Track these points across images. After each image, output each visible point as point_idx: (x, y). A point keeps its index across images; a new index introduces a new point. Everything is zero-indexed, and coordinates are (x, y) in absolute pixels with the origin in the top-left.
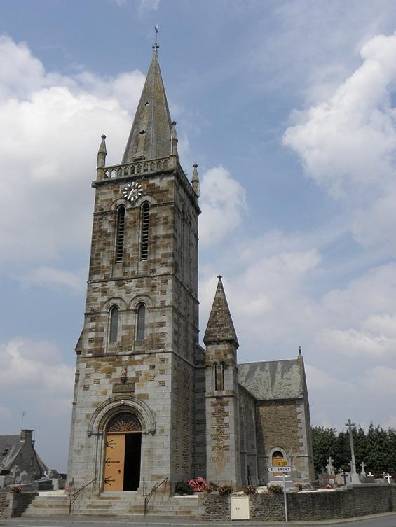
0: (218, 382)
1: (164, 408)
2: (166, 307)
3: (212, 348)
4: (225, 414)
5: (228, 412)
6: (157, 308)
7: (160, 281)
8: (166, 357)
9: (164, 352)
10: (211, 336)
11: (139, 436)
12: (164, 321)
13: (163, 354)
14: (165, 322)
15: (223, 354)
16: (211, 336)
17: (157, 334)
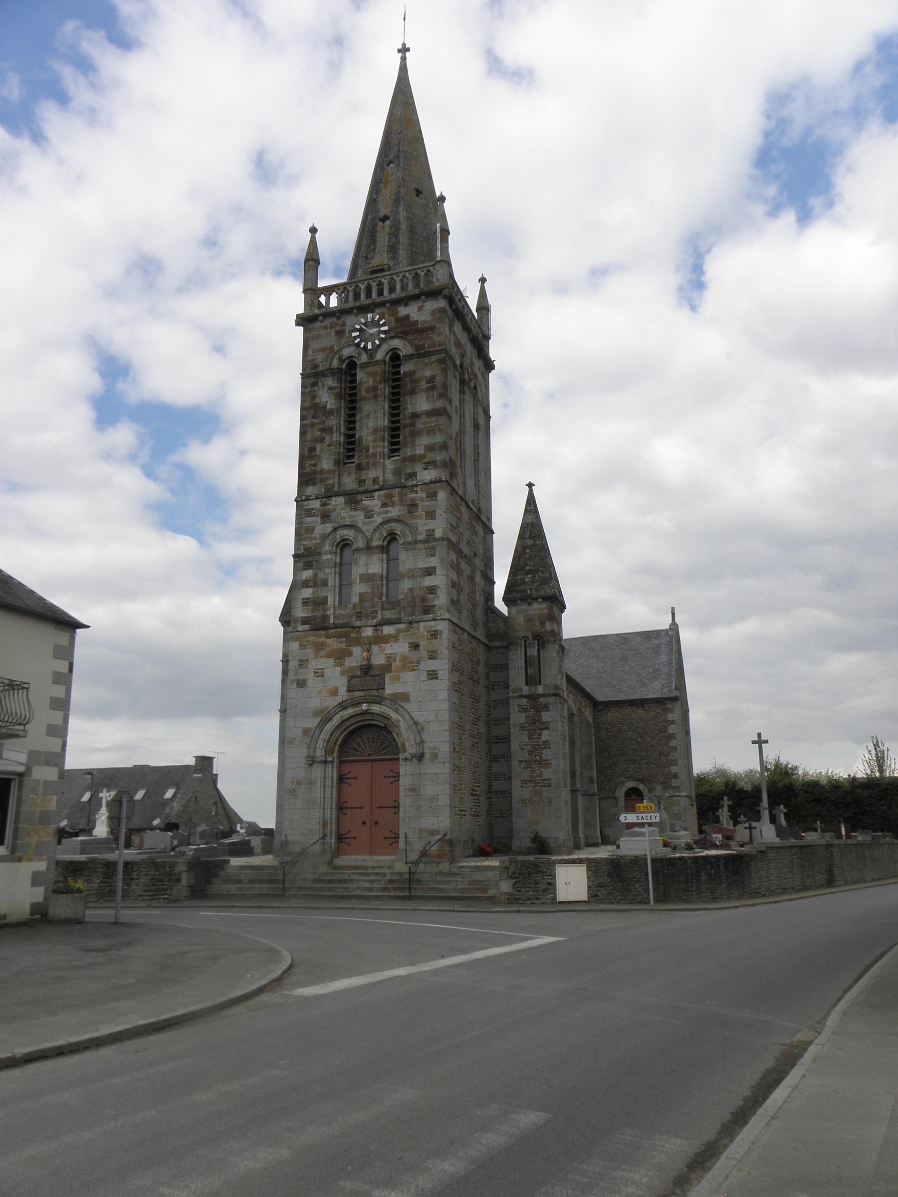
0: (529, 671)
1: (437, 716)
2: (436, 540)
6: (421, 542)
7: (424, 495)
8: (439, 628)
9: (434, 620)
10: (517, 592)
13: (433, 623)
14: (435, 568)
15: (537, 622)
17: (420, 588)
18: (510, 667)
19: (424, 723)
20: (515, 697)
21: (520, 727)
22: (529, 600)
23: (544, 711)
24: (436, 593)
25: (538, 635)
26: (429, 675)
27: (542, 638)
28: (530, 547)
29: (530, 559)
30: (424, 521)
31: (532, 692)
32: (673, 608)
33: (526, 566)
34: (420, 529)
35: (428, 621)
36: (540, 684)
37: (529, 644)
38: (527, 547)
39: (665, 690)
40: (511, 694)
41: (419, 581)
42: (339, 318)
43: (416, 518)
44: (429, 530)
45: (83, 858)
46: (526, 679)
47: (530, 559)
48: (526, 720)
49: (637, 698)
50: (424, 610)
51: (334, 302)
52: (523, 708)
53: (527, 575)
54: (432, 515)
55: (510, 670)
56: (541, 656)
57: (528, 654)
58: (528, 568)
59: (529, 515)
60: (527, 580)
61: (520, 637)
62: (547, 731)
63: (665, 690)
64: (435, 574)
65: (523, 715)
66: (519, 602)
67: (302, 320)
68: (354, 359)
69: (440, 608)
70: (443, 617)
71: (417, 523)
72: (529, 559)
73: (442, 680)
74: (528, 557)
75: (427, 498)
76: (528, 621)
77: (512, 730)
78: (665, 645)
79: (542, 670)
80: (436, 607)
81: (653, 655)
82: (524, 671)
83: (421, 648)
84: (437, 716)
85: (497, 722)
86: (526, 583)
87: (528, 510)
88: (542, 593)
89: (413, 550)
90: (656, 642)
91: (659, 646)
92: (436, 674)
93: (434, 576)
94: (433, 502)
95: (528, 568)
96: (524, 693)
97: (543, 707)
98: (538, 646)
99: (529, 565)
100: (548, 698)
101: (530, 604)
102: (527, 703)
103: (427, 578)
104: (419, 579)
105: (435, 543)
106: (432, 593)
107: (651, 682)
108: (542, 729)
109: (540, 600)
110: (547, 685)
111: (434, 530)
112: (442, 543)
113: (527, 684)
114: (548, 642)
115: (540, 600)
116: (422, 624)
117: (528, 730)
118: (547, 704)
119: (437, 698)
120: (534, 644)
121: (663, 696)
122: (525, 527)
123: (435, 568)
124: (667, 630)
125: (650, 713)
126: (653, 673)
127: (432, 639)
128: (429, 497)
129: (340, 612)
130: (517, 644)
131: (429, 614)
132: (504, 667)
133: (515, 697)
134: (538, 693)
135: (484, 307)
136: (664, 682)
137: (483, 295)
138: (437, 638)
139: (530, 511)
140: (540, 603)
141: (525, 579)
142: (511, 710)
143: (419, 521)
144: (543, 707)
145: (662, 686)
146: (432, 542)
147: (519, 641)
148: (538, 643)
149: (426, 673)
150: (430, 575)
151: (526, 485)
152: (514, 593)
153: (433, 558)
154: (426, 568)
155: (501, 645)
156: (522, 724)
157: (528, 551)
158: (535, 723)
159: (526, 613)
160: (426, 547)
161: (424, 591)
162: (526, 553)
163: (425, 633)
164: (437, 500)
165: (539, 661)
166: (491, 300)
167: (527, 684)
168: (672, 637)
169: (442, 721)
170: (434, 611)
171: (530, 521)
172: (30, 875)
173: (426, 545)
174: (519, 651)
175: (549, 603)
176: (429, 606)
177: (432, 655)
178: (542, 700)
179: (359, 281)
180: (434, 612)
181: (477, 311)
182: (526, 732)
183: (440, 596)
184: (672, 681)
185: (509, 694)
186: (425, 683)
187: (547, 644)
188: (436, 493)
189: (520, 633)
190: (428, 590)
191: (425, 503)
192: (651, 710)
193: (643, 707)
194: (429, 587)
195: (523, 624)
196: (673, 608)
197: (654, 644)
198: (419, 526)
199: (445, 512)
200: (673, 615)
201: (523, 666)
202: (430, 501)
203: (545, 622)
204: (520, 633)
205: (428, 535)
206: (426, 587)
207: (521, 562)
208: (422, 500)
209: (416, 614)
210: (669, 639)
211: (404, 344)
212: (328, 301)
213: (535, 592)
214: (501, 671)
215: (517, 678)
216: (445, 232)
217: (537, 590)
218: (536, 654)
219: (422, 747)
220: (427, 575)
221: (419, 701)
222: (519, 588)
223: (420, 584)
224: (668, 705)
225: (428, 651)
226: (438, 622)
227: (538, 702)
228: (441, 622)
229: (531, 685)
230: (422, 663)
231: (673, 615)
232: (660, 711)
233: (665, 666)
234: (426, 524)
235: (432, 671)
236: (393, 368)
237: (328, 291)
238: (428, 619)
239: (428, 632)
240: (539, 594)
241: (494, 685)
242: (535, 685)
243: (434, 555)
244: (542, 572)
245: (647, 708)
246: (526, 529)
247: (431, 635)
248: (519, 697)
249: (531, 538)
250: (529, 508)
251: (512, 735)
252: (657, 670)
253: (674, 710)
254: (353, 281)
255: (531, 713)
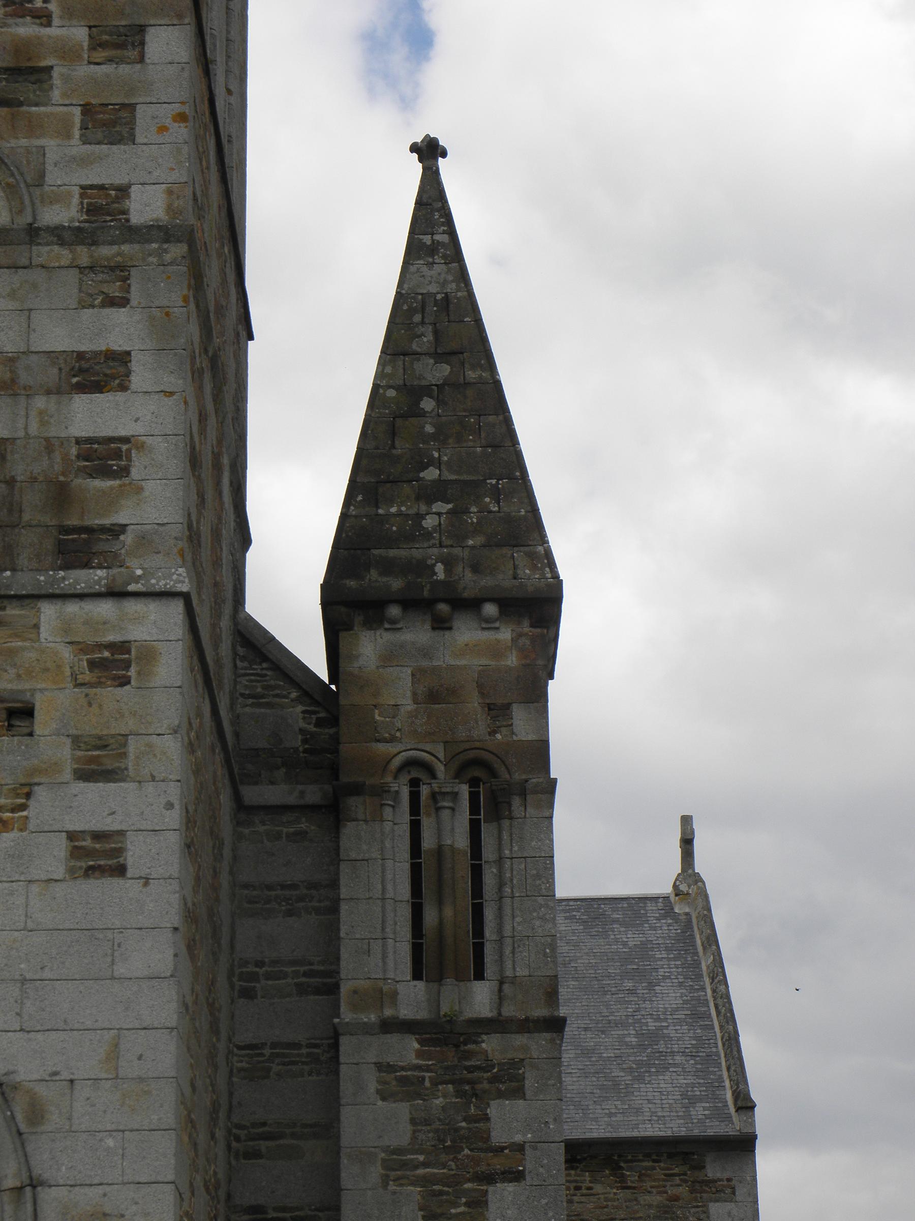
0: (430, 917)
1: (114, 1053)
2: (133, 233)
3: (389, 658)
4: (498, 1163)
5: (520, 1148)
6: (58, 234)
7: (80, 34)
8: (137, 633)
9: (117, 594)
10: (388, 567)
11: (483, 944)
12: (117, 344)
13: (105, 609)
14: (123, 358)
15: (473, 704)
16: (388, 567)
17: (49, 445)
18: (344, 892)
19: (41, 1090)
20: (366, 1029)
21: (387, 1165)
22: (443, 607)
23: (501, 1095)
24: (125, 471)
25: (478, 762)
26: (76, 852)
27: (493, 773)
28: (439, 391)
29: (441, 436)
30: (76, 147)
31: (445, 1009)
32: (686, 821)
33: (425, 467)
34: (54, 177)
35: (81, 596)
36: (480, 975)
37: (434, 796)
38: (426, 390)
39: (700, 1110)
40: (347, 1015)
41: (41, 413)
43: (34, 128)
44: (102, 187)
46: (417, 951)
47: (441, 436)
48: (414, 1138)
49: (595, 1135)
50: (60, 543)
52: (403, 1081)
53: (430, 501)
54: (114, 123)
55: (344, 907)
56: (488, 852)
57: (428, 842)
58: (431, 474)
59: (431, 265)
60: (429, 522)
61: (396, 762)
62: (510, 1187)
63: (700, 1110)
64: (123, 388)
65: (403, 1110)
66: (394, 611)
69: (144, 542)
70: (161, 585)
71: (42, 150)
72: (434, 437)
73: (146, 881)
74: (429, 429)
75: (92, 48)
76: (433, 697)
77: (346, 1180)
78: (668, 950)
79: (489, 914)
80: (128, 538)
81: (629, 984)
82: (405, 913)
83: (43, 723)
84: (114, 1053)
85: (263, 1145)
86: (428, 535)
87: (422, 244)
88: (502, 580)
89: (16, 267)
90: (633, 938)
91: (644, 949)
92: (119, 851)
93: (120, 396)
94: (125, 70)
95: (431, 474)
96: (406, 1012)
97: (494, 1080)
98: (474, 808)
99: (438, 464)
100: (519, 1040)
101: (441, 624)
103: (81, 403)
104: (40, 402)
105: (125, 248)
106: (105, 472)
107: (640, 1079)
108: (489, 1179)
109: (490, 609)
110: (514, 980)
111: (123, 191)
112: (160, 253)
113: (417, 975)
114: (523, 794)
115: (490, 609)
116: (48, 612)
117: (425, 1181)
118: (516, 1064)
119: (120, 970)
120: (455, 796)
121: (696, 1132)
122: (412, 311)
123: (123, 358)
124: (666, 898)
125: (645, 1199)
126: (642, 1047)
127: (99, 684)
128: (102, 45)
130: (380, 792)
131: (87, 565)
132: (301, 899)
133: (366, 1029)
134: (469, 1014)
136: (690, 1080)
138: (124, 682)
139: (433, 249)
140: (488, 624)
141: (421, 517)
142: (346, 1088)
143: (50, 143)
144: (494, 1080)
145: (684, 1095)
146: (112, 243)
147: (389, 779)
148: (474, 798)
149: (61, 846)
150: (98, 387)
151: (414, 148)
152: (374, 574)
153: (119, 315)
154: (81, 356)
155: (292, 800)
156: (398, 1151)
157: (428, 404)
158: (455, 1149)
159: (425, 663)
160: (84, 261)
161: (65, 458)
162: (422, 414)
163: (67, 654)
164: (141, 59)
165: (477, 872)
167: (417, 975)
168: (689, 921)
169: (141, 1080)
170: (116, 555)
171: (433, 289)
172: (680, 817)
173: (84, 255)
174: (388, 826)
175: (526, 627)
176: (89, 530)
177: (91, 760)
178: (491, 1044)
180: (112, 560)
182: (415, 1190)
183: (150, 487)
184: (720, 1080)
185: (338, 1016)
186: (59, 890)
187: (516, 802)
188: (141, 29)
189: (392, 749)
190: (85, 456)
191: (83, 71)
192: (648, 1184)
193: (616, 1169)
194: (90, 440)
195: (408, 705)
196: (686, 821)
197: (625, 944)
198: (49, 167)
199: (181, 118)
200: (687, 843)
201: (404, 890)
202: (110, 60)
203: (507, 707)
204: (392, 749)
205: (92, 210)
206: (78, 441)
207: (402, 447)
208: (68, 53)
209: (23, 560)
210: (676, 930)
213: (469, 575)
214: (290, 913)
215: (376, 947)
217: (476, 568)
218: (462, 842)
219: (29, 1207)
220: (82, 388)
221: (24, 981)
222: (392, 553)
223: (43, 423)
224: (714, 1170)
225: (76, 741)
226: (133, 607)
227: (468, 1055)
228: (152, 610)
229: (439, 979)
230: (40, 793)
231: (687, 843)
232: (683, 1191)
233: (680, 1022)
234: (84, 162)
235: (98, 836)
238: (81, 587)
239: (82, 648)
240: (486, 581)
241: (254, 977)
242: (461, 977)
243: (122, 302)
244: (496, 493)
245: (632, 1177)
246: (417, 318)
247: (92, 664)
248: (389, 1026)
249: (440, 356)
250: (427, 239)
251: (346, 1197)
252: (655, 1036)
253: (733, 1189)
255: (439, 1102)
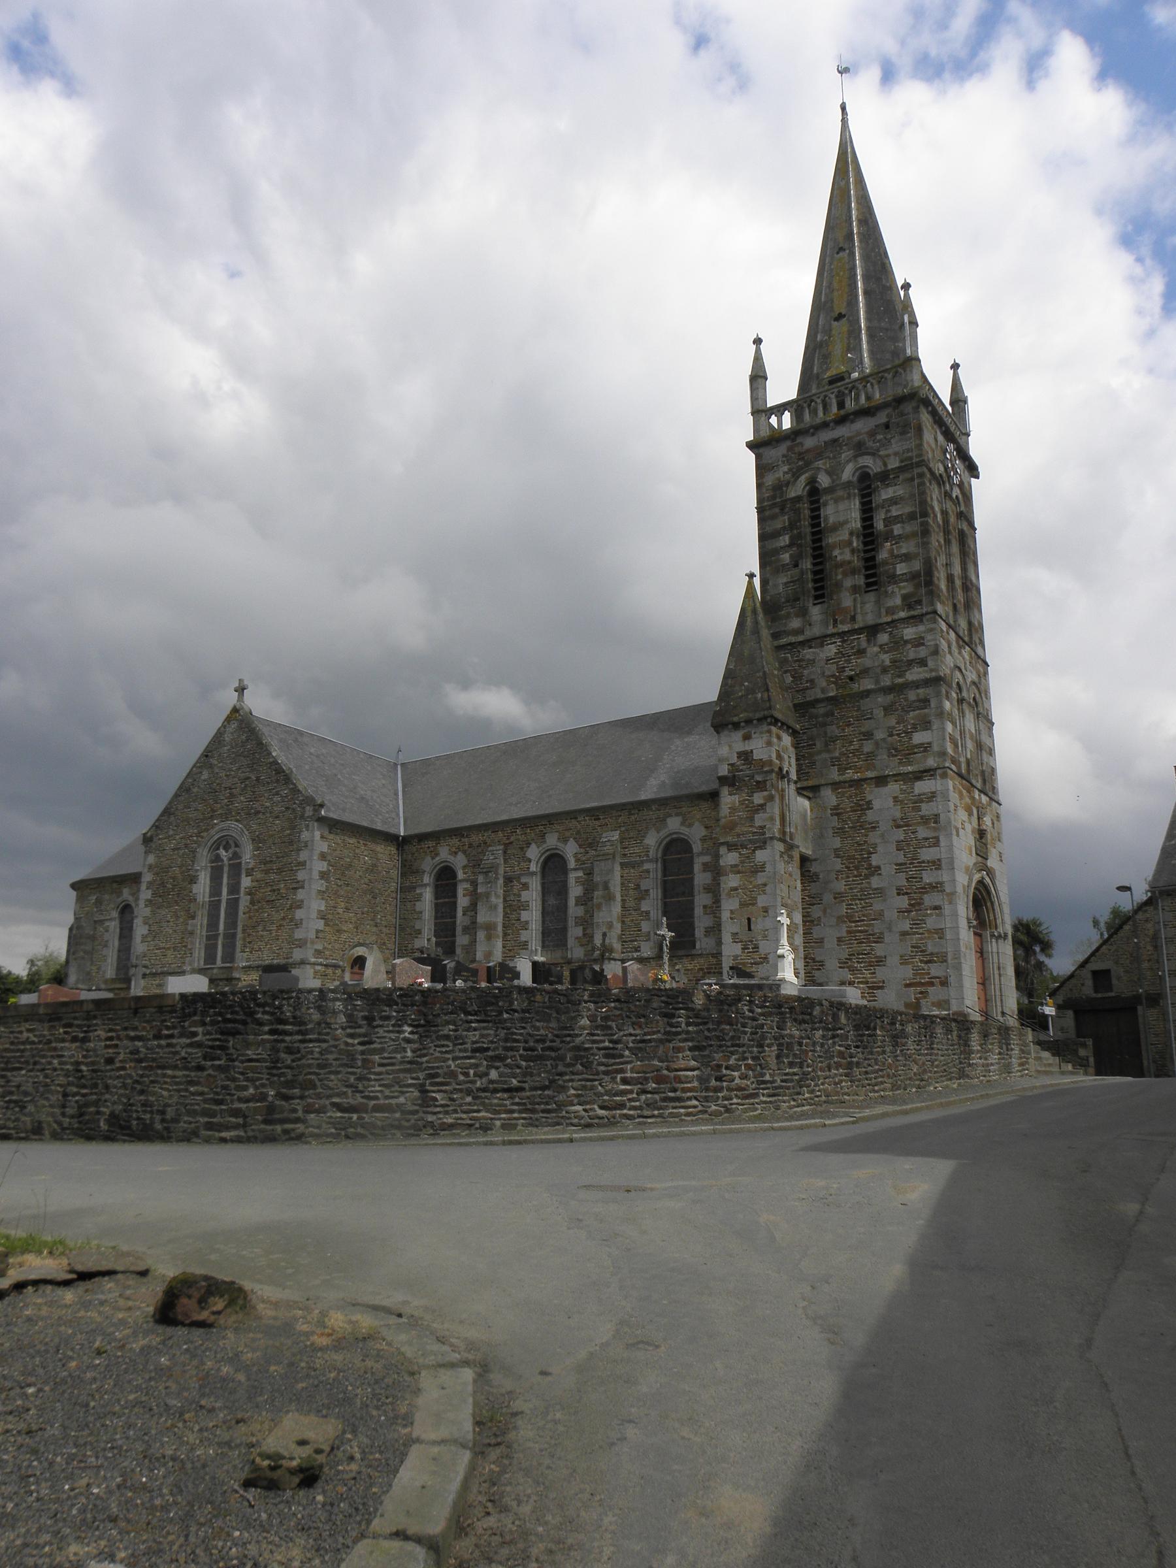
42: (793, 440)
45: (110, 995)
51: (787, 421)
67: (751, 446)
68: (867, 470)
102: (412, 1033)
129: (595, 1063)
135: (959, 400)
137: (956, 386)
166: (967, 392)
179: (814, 395)
181: (952, 404)
211: (874, 461)
212: (780, 422)
216: (914, 323)
236: (812, 504)
237: (779, 409)
254: (821, 390)
